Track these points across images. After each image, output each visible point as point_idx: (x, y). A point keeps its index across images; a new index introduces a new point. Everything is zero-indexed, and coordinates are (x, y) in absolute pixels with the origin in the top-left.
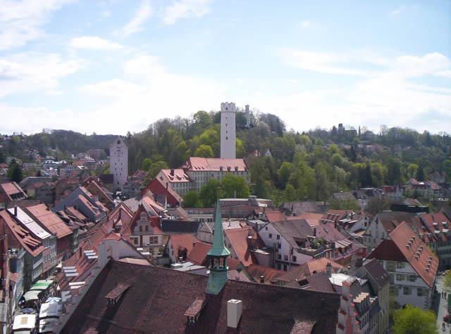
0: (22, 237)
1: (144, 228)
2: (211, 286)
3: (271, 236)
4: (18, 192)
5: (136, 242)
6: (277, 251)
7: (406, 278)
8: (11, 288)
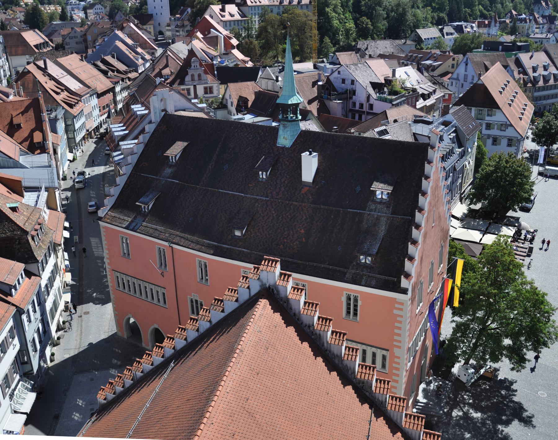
0: (58, 93)
1: (196, 78)
2: (282, 137)
3: (344, 81)
4: (42, 41)
5: (189, 93)
6: (351, 98)
7: (496, 127)
8: (55, 152)
